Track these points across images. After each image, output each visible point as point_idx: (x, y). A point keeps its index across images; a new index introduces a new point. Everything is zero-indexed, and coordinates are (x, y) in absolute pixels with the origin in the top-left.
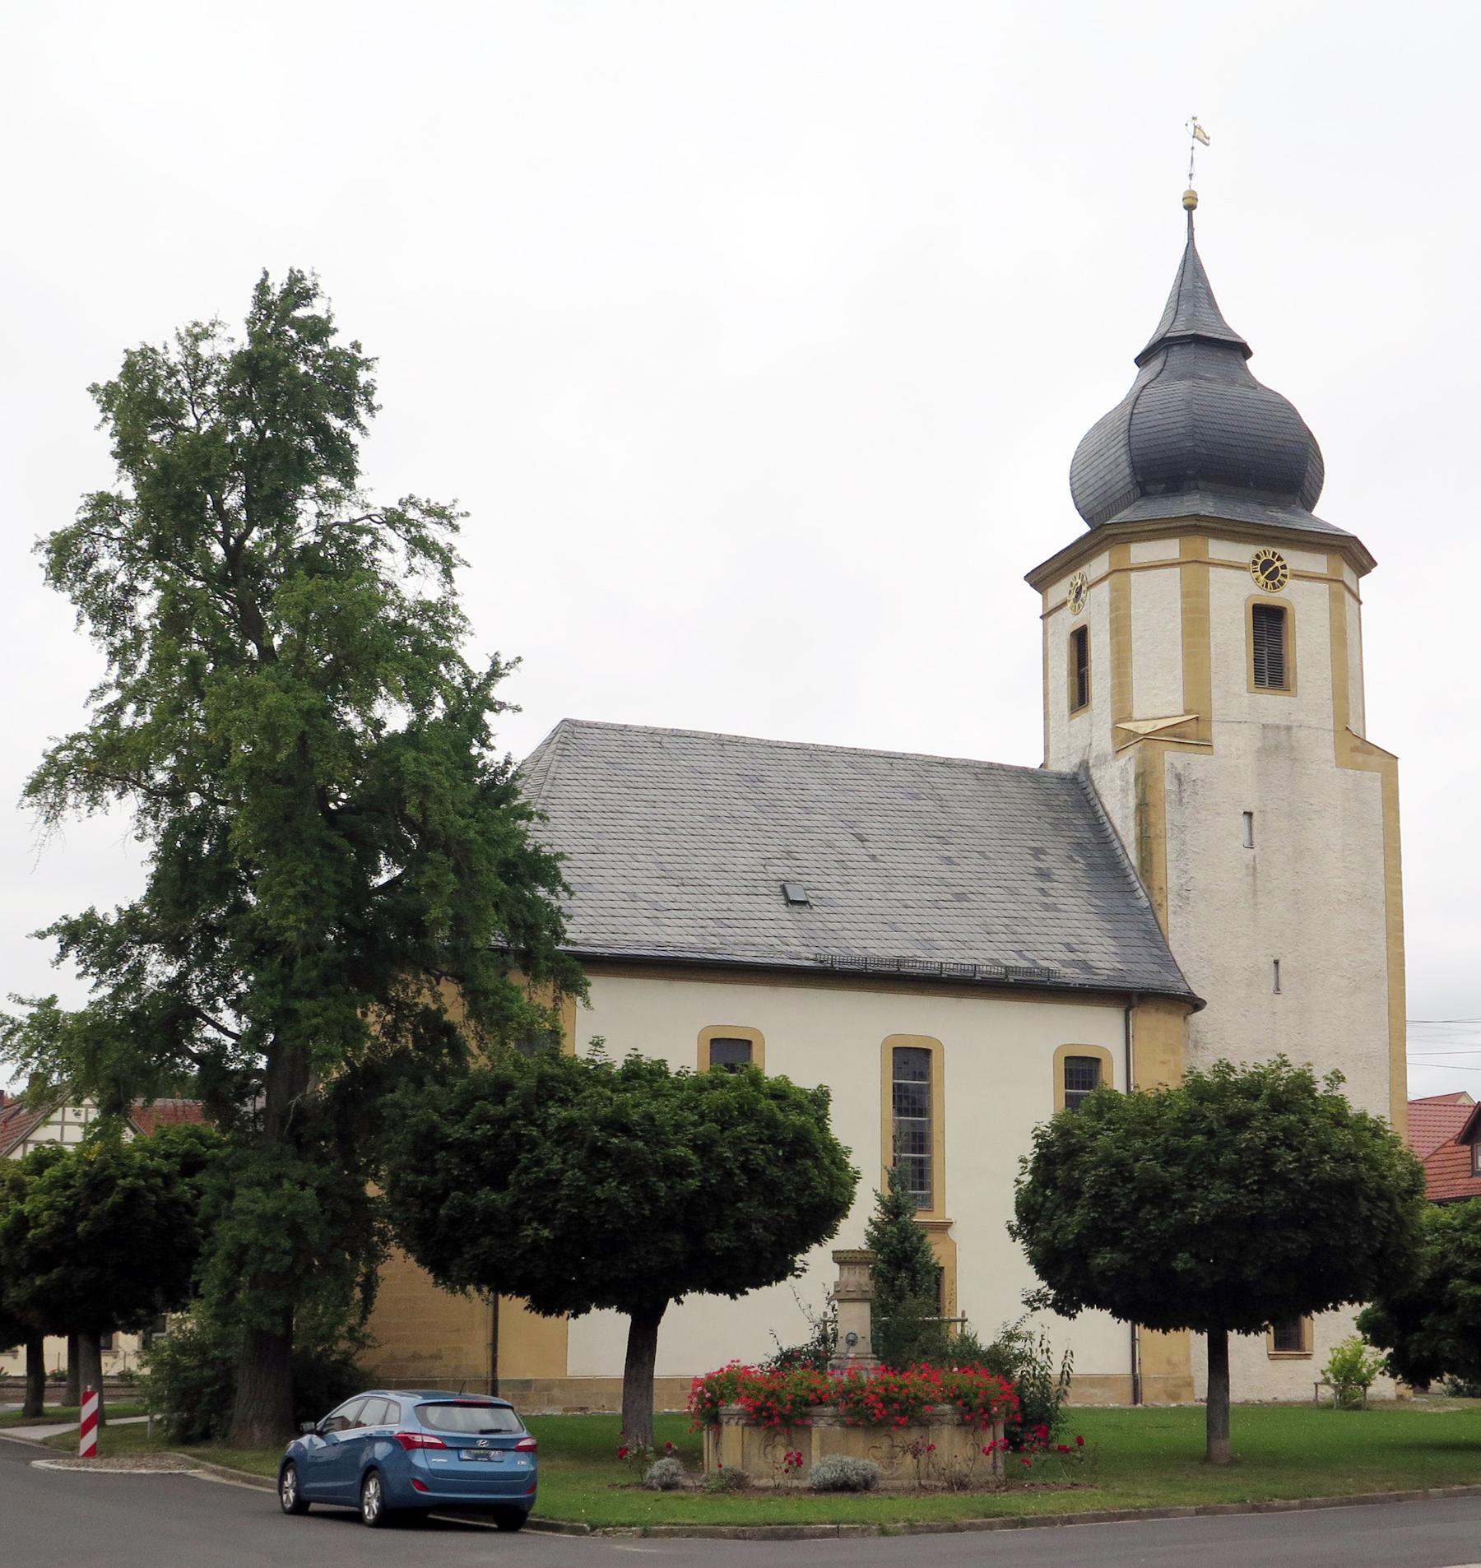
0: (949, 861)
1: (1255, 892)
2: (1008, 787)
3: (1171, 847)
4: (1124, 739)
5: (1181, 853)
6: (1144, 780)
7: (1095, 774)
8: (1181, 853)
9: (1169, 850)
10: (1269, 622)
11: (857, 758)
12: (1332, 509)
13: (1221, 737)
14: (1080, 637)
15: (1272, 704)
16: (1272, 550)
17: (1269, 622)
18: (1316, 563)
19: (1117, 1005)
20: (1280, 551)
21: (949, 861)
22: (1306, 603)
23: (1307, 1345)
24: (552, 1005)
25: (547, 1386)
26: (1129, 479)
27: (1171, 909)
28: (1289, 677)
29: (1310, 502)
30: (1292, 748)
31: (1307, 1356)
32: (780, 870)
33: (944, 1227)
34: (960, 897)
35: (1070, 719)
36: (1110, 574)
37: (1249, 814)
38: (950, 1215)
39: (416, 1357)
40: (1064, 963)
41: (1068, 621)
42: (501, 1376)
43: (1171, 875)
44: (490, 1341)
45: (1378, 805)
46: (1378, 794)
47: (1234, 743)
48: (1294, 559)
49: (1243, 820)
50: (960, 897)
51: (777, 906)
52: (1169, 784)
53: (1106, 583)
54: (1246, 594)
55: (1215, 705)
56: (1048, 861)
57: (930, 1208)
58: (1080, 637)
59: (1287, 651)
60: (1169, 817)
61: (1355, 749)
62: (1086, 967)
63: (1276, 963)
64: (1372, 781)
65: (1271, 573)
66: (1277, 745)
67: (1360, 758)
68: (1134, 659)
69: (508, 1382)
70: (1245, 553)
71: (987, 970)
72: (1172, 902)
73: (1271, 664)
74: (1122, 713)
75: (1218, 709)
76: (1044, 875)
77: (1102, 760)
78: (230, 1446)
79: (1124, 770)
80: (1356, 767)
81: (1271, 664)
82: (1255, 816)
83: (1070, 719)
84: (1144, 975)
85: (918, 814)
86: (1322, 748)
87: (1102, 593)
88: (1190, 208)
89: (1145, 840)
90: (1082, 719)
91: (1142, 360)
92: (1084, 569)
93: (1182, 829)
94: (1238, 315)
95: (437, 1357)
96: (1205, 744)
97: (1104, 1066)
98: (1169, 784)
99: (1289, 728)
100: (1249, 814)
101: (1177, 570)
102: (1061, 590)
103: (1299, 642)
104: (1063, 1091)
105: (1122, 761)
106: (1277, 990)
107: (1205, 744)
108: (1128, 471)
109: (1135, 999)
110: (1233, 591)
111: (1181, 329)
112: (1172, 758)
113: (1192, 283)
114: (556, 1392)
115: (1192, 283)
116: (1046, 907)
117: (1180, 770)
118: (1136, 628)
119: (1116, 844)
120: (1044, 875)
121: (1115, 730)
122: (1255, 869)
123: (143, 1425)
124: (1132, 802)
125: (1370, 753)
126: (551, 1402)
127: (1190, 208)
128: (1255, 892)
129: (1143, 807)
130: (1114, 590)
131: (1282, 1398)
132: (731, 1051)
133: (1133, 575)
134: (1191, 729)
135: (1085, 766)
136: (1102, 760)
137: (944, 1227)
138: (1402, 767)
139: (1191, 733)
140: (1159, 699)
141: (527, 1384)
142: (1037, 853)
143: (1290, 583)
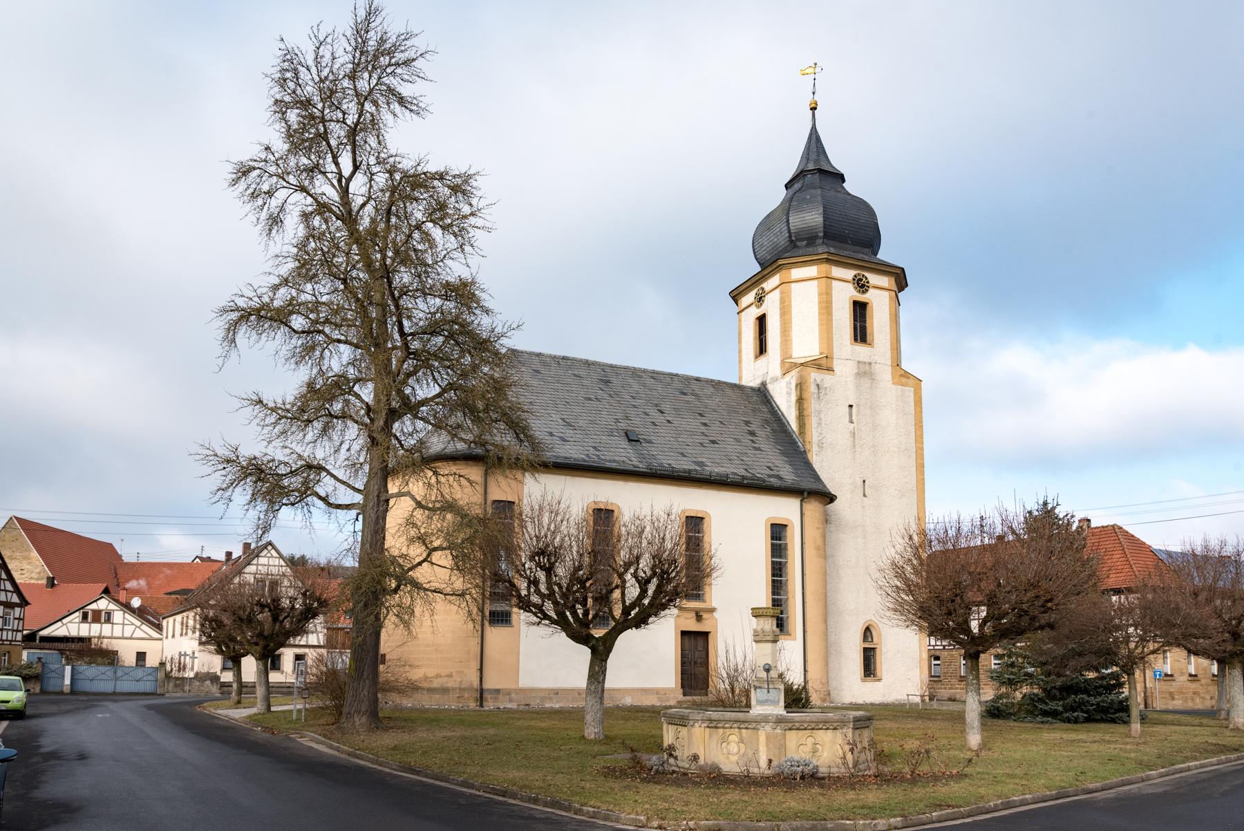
0: (705, 425)
2: (729, 392)
4: (788, 366)
5: (819, 424)
6: (801, 386)
7: (770, 387)
8: (819, 424)
9: (812, 423)
10: (860, 309)
11: (655, 375)
12: (885, 254)
13: (837, 365)
14: (762, 320)
15: (861, 349)
17: (860, 309)
18: (884, 281)
20: (866, 274)
21: (705, 425)
22: (879, 300)
25: (508, 693)
28: (868, 338)
29: (876, 254)
30: (871, 374)
31: (879, 680)
32: (623, 425)
33: (712, 610)
34: (714, 442)
37: (851, 406)
38: (714, 605)
40: (770, 476)
41: (755, 312)
42: (485, 686)
46: (912, 398)
47: (844, 368)
48: (873, 279)
50: (714, 442)
51: (624, 443)
52: (813, 389)
55: (835, 350)
56: (753, 427)
57: (704, 601)
58: (762, 320)
59: (868, 325)
60: (812, 405)
61: (902, 376)
62: (780, 478)
64: (910, 392)
65: (862, 285)
66: (865, 372)
67: (904, 380)
70: (849, 274)
71: (732, 478)
72: (815, 449)
73: (861, 334)
75: (836, 353)
76: (752, 433)
77: (775, 380)
78: (983, 724)
79: (789, 383)
80: (902, 385)
81: (861, 334)
84: (807, 484)
86: (885, 373)
88: (813, 109)
89: (801, 417)
90: (763, 359)
91: (788, 186)
92: (764, 285)
94: (838, 159)
95: (450, 676)
96: (830, 369)
98: (813, 389)
102: (749, 298)
104: (769, 541)
105: (788, 377)
107: (830, 369)
110: (844, 294)
112: (814, 376)
113: (815, 144)
114: (513, 695)
115: (815, 144)
116: (756, 449)
118: (794, 311)
120: (752, 433)
121: (783, 362)
123: (291, 711)
124: (794, 398)
126: (511, 701)
127: (813, 109)
129: (800, 401)
130: (782, 293)
131: (868, 701)
132: (603, 516)
134: (824, 362)
135: (764, 384)
136: (775, 380)
137: (712, 610)
139: (823, 364)
140: (806, 346)
141: (498, 691)
142: (747, 423)
143: (871, 291)
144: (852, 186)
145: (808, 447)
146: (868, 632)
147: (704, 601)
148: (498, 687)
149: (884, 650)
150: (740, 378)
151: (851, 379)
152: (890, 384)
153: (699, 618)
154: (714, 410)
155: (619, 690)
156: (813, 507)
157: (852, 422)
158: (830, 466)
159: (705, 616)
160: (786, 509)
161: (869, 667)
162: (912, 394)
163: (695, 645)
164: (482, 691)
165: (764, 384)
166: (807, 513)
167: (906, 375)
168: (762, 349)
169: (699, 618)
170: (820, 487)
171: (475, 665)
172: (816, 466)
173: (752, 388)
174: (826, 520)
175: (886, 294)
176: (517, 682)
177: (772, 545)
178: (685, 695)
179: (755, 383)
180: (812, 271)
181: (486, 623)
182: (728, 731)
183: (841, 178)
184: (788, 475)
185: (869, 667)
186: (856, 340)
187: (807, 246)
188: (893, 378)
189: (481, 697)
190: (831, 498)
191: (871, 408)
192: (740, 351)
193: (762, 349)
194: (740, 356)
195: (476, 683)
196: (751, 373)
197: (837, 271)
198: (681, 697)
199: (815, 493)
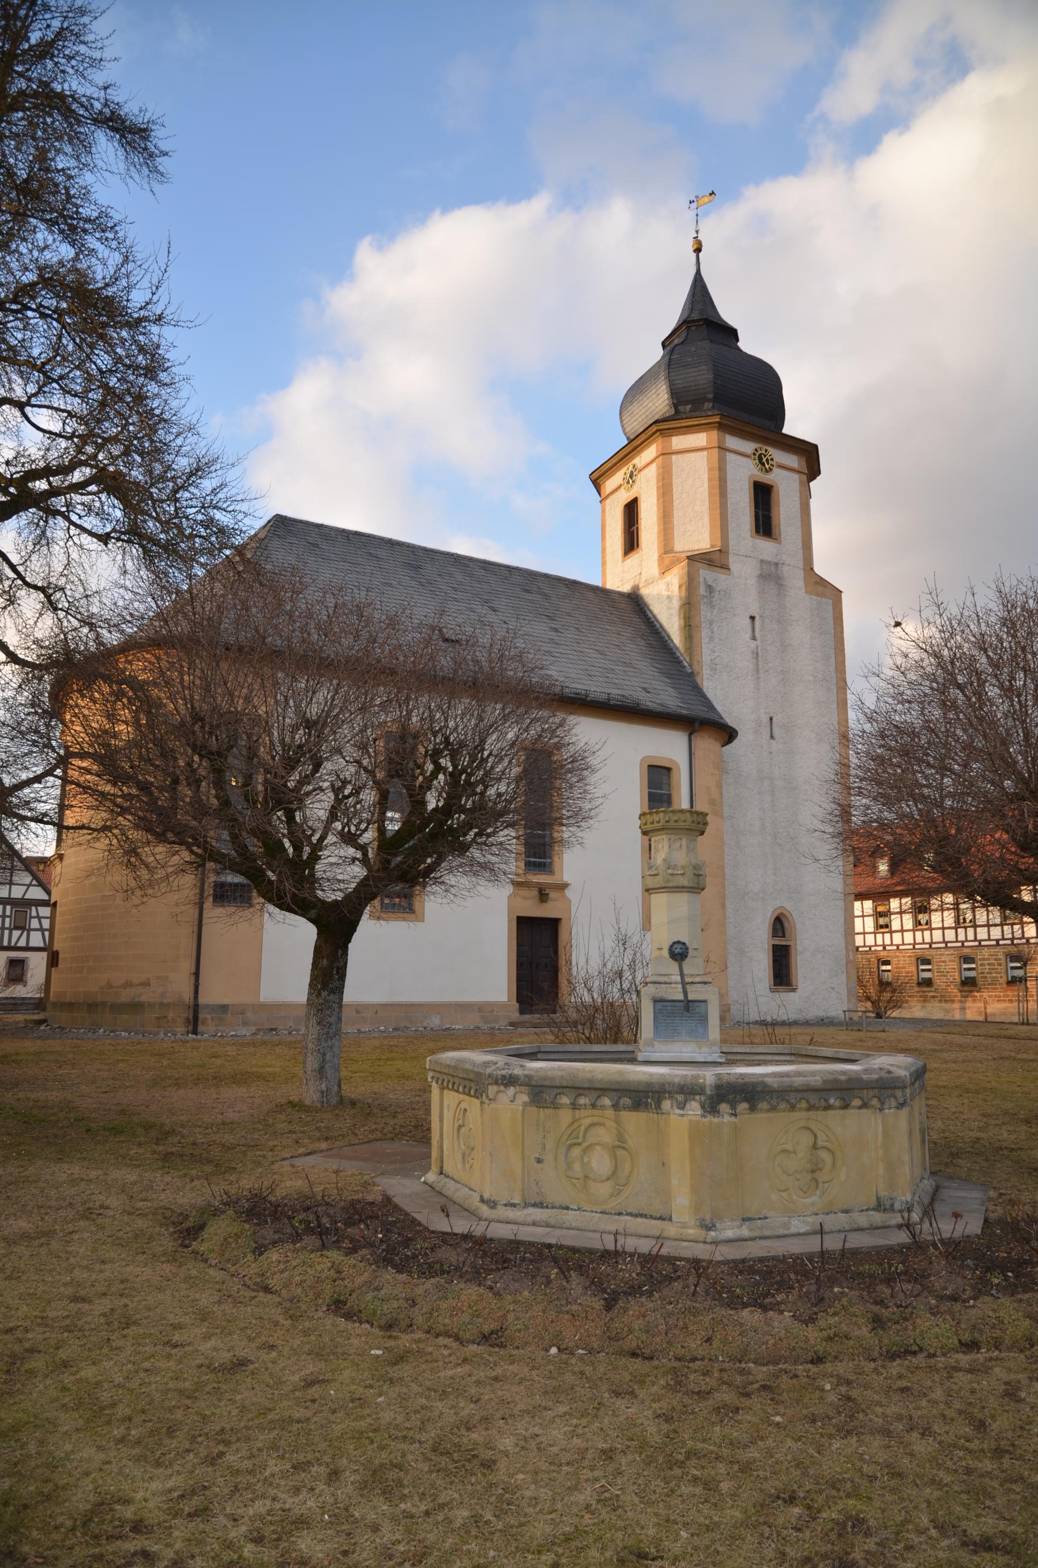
1: (758, 670)
2: (590, 595)
3: (704, 633)
8: (711, 639)
12: (793, 427)
14: (631, 510)
15: (765, 547)
16: (765, 447)
18: (792, 460)
19: (683, 730)
20: (769, 449)
21: (556, 630)
22: (785, 484)
23: (794, 982)
24: (60, 167)
25: (241, 1010)
26: (667, 402)
27: (705, 676)
28: (774, 531)
31: (794, 990)
33: (563, 887)
35: (623, 561)
36: (657, 457)
38: (567, 878)
39: (128, 984)
42: (202, 1000)
43: (707, 653)
44: (193, 970)
45: (831, 620)
47: (743, 570)
48: (779, 456)
49: (749, 621)
52: (702, 591)
53: (654, 465)
54: (750, 473)
55: (731, 543)
57: (551, 872)
58: (631, 510)
59: (774, 514)
61: (816, 583)
63: (771, 719)
64: (827, 604)
65: (761, 460)
66: (771, 575)
67: (820, 589)
68: (675, 512)
69: (208, 1006)
72: (706, 672)
73: (764, 524)
74: (667, 547)
80: (817, 595)
81: (764, 524)
82: (757, 619)
83: (623, 561)
84: (698, 711)
85: (531, 601)
86: (796, 581)
87: (652, 471)
88: (698, 251)
89: (689, 627)
90: (634, 558)
93: (711, 623)
94: (728, 313)
95: (146, 984)
96: (725, 567)
97: (674, 773)
98: (702, 591)
99: (776, 564)
100: (753, 618)
101: (705, 453)
103: (782, 509)
104: (646, 791)
106: (772, 737)
108: (666, 396)
109: (697, 725)
110: (743, 472)
111: (695, 316)
112: (705, 574)
113: (699, 291)
115: (699, 291)
117: (710, 583)
119: (664, 634)
122: (757, 654)
125: (826, 587)
126: (245, 1023)
128: (758, 670)
133: (674, 457)
136: (649, 583)
137: (563, 887)
138: (844, 597)
139: (713, 560)
140: (697, 535)
141: (224, 1008)
143: (775, 470)
144: (746, 344)
145: (696, 668)
146: (779, 925)
147: (551, 872)
148: (226, 1001)
149: (799, 948)
150: (604, 583)
151: (752, 582)
152: (802, 593)
153: (543, 896)
154: (568, 614)
155: (420, 1006)
156: (706, 744)
157: (754, 638)
158: (727, 693)
159: (553, 895)
160: (669, 746)
161: (782, 972)
162: (830, 608)
163: (538, 945)
164: (196, 1007)
165: (636, 588)
166: (698, 753)
167: (822, 582)
168: (631, 543)
169: (543, 896)
170: (716, 718)
171: (187, 966)
172: (710, 694)
173: (620, 594)
174: (721, 767)
175: (796, 476)
176: (257, 992)
177: (650, 794)
178: (522, 1012)
179: (626, 588)
180: (700, 439)
181: (208, 904)
182: (586, 1117)
183: (732, 333)
184: (668, 698)
185: (782, 972)
186: (757, 531)
187: (691, 411)
188: (806, 586)
189: (196, 1019)
190: (728, 734)
191: (779, 622)
192: (604, 550)
193: (631, 543)
194: (604, 557)
195: (187, 996)
196: (619, 576)
197: (732, 442)
198: (515, 1016)
199: (706, 724)
